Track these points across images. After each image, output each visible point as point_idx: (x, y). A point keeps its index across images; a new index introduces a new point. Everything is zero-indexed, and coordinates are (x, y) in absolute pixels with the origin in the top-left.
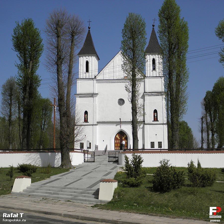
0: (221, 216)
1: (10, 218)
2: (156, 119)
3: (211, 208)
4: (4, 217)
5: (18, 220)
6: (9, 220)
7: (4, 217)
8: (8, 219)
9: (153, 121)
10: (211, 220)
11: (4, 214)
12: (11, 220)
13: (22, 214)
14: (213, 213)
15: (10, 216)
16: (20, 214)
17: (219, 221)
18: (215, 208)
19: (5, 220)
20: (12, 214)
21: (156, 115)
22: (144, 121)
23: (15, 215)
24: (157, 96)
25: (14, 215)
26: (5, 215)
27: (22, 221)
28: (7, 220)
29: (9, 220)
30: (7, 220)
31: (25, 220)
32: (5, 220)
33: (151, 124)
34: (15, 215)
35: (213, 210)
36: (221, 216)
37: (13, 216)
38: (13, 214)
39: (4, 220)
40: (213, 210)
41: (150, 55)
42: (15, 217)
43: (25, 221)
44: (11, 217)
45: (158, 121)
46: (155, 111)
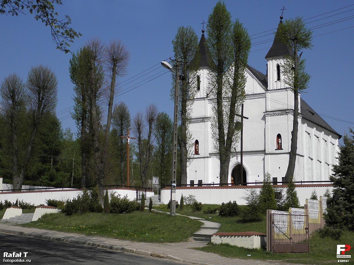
0: (350, 256)
1: (12, 258)
2: (280, 147)
3: (339, 246)
4: (4, 256)
5: (22, 261)
6: (10, 261)
7: (4, 256)
8: (9, 259)
9: (275, 150)
10: (339, 260)
11: (5, 253)
12: (13, 261)
13: (26, 253)
14: (341, 252)
15: (12, 255)
16: (24, 253)
17: (342, 261)
18: (344, 246)
19: (6, 261)
20: (14, 254)
21: (280, 142)
22: (265, 150)
23: (18, 254)
24: (281, 115)
25: (16, 254)
26: (5, 254)
27: (26, 262)
28: (9, 261)
29: (10, 261)
30: (8, 260)
31: (30, 261)
32: (6, 261)
33: (274, 153)
34: (18, 254)
35: (341, 248)
36: (350, 256)
37: (15, 255)
38: (16, 253)
39: (5, 260)
40: (341, 248)
41: (274, 60)
42: (18, 257)
43: (29, 261)
44: (14, 256)
45: (282, 149)
46: (279, 136)
